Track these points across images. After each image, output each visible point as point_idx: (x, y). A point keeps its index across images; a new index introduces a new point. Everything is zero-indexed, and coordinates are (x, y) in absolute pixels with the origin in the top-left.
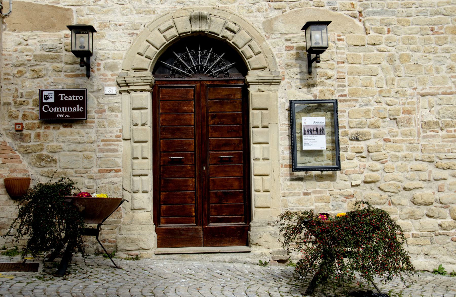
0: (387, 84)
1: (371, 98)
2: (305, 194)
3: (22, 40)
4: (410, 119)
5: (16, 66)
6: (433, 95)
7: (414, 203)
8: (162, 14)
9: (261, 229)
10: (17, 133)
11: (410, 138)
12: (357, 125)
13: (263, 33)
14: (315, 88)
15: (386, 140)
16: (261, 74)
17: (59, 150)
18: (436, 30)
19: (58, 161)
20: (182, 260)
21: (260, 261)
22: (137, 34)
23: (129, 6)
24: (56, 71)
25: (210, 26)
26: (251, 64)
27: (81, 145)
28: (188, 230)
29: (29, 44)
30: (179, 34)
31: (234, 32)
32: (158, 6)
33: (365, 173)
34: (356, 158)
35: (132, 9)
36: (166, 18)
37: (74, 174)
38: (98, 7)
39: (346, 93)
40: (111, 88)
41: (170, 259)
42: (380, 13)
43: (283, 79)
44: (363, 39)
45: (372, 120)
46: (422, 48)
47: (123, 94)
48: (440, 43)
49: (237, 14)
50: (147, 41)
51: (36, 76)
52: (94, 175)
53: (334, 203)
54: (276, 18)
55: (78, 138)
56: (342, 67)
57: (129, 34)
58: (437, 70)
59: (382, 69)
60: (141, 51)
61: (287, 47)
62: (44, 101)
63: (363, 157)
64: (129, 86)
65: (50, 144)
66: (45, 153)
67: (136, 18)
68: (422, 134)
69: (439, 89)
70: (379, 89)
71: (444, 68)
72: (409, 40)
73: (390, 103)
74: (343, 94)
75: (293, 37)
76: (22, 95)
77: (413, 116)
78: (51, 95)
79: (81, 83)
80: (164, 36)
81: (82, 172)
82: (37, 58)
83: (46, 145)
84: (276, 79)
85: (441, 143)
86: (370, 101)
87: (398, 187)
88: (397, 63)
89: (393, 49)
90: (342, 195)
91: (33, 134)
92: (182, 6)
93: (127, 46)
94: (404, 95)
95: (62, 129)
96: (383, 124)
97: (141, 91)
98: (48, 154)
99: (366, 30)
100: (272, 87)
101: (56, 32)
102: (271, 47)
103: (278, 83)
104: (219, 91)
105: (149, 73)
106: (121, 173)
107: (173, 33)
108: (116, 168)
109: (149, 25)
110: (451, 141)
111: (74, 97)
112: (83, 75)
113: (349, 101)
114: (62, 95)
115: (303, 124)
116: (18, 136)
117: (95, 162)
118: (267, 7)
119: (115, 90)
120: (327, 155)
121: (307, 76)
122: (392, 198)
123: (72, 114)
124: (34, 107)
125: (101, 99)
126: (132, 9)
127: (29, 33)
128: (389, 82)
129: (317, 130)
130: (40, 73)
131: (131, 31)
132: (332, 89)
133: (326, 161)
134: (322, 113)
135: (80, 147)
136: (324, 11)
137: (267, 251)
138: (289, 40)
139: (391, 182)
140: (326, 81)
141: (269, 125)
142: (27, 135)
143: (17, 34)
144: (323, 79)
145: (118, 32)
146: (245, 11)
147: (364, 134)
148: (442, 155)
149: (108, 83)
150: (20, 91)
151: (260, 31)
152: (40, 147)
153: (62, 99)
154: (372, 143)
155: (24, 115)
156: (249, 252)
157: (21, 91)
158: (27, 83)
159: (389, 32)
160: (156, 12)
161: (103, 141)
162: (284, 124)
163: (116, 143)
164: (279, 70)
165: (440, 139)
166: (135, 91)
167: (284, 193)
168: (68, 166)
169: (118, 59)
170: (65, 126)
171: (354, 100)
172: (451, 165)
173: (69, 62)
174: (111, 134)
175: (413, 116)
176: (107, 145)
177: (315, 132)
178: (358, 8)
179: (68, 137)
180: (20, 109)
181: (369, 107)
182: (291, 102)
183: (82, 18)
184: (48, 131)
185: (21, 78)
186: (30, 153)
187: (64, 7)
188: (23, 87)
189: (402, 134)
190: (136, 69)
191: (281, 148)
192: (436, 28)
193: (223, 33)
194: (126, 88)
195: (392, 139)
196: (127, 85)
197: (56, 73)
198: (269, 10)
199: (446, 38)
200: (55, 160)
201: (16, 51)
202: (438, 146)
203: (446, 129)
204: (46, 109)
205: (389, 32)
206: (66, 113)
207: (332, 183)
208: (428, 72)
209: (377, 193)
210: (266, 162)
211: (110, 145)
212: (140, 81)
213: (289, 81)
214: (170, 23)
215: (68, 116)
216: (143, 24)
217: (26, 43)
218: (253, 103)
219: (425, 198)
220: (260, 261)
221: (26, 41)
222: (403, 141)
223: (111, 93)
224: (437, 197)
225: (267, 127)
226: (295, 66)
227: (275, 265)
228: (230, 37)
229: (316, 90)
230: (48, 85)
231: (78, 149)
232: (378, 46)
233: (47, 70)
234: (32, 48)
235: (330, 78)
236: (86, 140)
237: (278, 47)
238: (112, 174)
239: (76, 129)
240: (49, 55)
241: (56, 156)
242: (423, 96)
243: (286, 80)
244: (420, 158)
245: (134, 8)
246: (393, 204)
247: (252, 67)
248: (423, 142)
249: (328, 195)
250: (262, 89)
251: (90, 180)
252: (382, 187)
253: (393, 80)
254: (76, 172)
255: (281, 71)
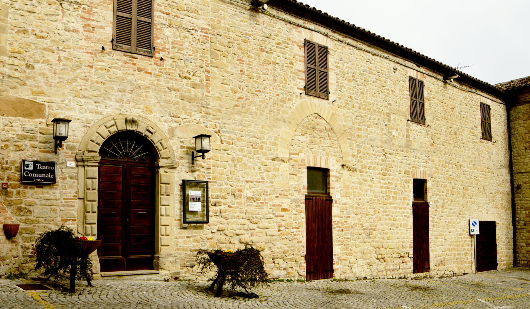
0: (231, 174)
1: (223, 181)
2: (188, 237)
3: (8, 123)
4: (241, 195)
5: (3, 141)
6: (252, 182)
7: (240, 243)
8: (106, 115)
9: (165, 259)
10: (3, 190)
11: (241, 206)
12: (216, 197)
13: (168, 136)
14: (195, 173)
15: (229, 206)
16: (167, 162)
17: (34, 204)
18: (254, 146)
19: (32, 212)
20: (118, 280)
21: (165, 279)
22: (89, 127)
23: (84, 107)
24: (33, 147)
25: (137, 128)
26: (161, 155)
27: (49, 201)
28: (117, 260)
29: (14, 126)
30: (118, 131)
31: (152, 133)
32: (104, 110)
33: (218, 226)
34: (214, 217)
35: (87, 109)
36: (109, 118)
37: (44, 222)
38: (64, 105)
39: (211, 177)
40: (71, 162)
41: (111, 279)
42: (228, 132)
43: (178, 166)
44: (220, 146)
45: (223, 194)
46: (247, 155)
47: (79, 167)
48: (255, 153)
49: (153, 122)
50: (97, 132)
51: (18, 150)
52: (58, 222)
53: (202, 243)
54: (176, 128)
55: (47, 196)
56: (209, 161)
57: (84, 126)
58: (254, 168)
59: (229, 165)
60: (94, 139)
61: (181, 146)
62: (26, 168)
63: (217, 216)
64: (84, 162)
65: (27, 199)
66: (23, 205)
67: (89, 116)
68: (246, 204)
69: (254, 179)
70: (227, 177)
71: (256, 167)
72: (242, 150)
73: (232, 185)
74: (209, 177)
75: (185, 141)
76: (7, 163)
77: (242, 193)
78: (31, 164)
79: (50, 157)
80: (109, 131)
81: (50, 220)
82: (19, 137)
83: (24, 200)
84: (175, 166)
85: (254, 209)
86: (223, 183)
87: (234, 233)
88: (236, 162)
89: (234, 154)
90: (207, 238)
91: (15, 191)
92: (119, 112)
93: (83, 134)
94: (239, 181)
95: (36, 189)
96: (228, 197)
97: (93, 166)
98: (25, 206)
99: (222, 141)
100: (172, 170)
101: (34, 119)
102: (172, 145)
103: (175, 168)
104: (137, 170)
105: (97, 154)
106: (76, 222)
107: (114, 129)
108: (73, 218)
109: (98, 122)
110: (258, 208)
111: (47, 167)
112: (52, 152)
113: (212, 182)
114: (38, 165)
115: (189, 195)
116: (4, 193)
117: (59, 213)
118: (171, 120)
119: (73, 164)
120: (200, 214)
121: (191, 165)
122: (231, 240)
123: (45, 179)
124: (16, 172)
125: (64, 169)
126: (87, 109)
127: (13, 118)
128: (232, 173)
129: (197, 198)
130: (21, 148)
131: (85, 125)
132: (204, 174)
133: (198, 218)
134: (198, 188)
135: (48, 203)
136: (202, 127)
137: (168, 273)
138: (183, 142)
139: (231, 231)
140: (201, 169)
141: (170, 194)
142: (10, 192)
143: (5, 118)
144: (200, 168)
145: (76, 124)
146: (157, 120)
147: (219, 203)
148: (254, 216)
149: (69, 159)
150: (6, 159)
151: (166, 134)
152: (19, 201)
153: (38, 168)
154: (222, 207)
155: (8, 177)
156: (158, 274)
157: (7, 160)
158: (11, 154)
159: (232, 144)
160: (102, 114)
161: (64, 199)
162: (177, 194)
163: (74, 201)
164: (176, 160)
165: (254, 207)
166: (88, 166)
167: (176, 237)
168: (40, 216)
169: (76, 142)
170: (38, 187)
171: (215, 182)
172: (257, 221)
173: (43, 142)
174: (70, 195)
175: (242, 193)
176: (67, 202)
177: (196, 200)
178: (218, 128)
179: (40, 195)
180: (5, 173)
181: (222, 187)
182: (183, 181)
183: (53, 111)
184: (26, 190)
185: (6, 150)
186: (12, 205)
187: (40, 102)
188: (8, 156)
189: (237, 203)
190: (89, 151)
191: (176, 209)
192: (254, 145)
193: (145, 133)
194: (82, 164)
195: (232, 206)
196: (83, 161)
197: (33, 149)
198: (171, 122)
199: (258, 151)
200: (30, 211)
201: (4, 130)
202: (253, 211)
203: (256, 202)
204: (27, 174)
205: (232, 144)
206: (41, 178)
207: (201, 231)
208: (250, 169)
209: (224, 237)
210: (167, 217)
211: (70, 202)
212: (92, 159)
213: (181, 167)
214: (113, 122)
215: (42, 180)
216: (94, 121)
217: (11, 125)
218: (162, 180)
219: (246, 240)
220: (165, 279)
221: (11, 123)
222: (237, 207)
223: (71, 166)
224: (251, 239)
225: (169, 195)
226: (185, 158)
227: (172, 281)
228: (150, 136)
229: (196, 174)
230: (26, 157)
231: (47, 204)
232: (227, 151)
233: (26, 146)
234: (16, 129)
235: (203, 167)
236: (52, 198)
237: (176, 146)
238: (71, 222)
239: (46, 190)
240: (28, 136)
241: (31, 208)
242: (247, 182)
243: (180, 167)
244: (244, 217)
245: (88, 109)
246: (231, 243)
247: (162, 157)
248: (246, 208)
249: (199, 238)
250: (167, 171)
251: (56, 226)
252: (226, 234)
253: (234, 172)
254: (45, 220)
255: (177, 160)
